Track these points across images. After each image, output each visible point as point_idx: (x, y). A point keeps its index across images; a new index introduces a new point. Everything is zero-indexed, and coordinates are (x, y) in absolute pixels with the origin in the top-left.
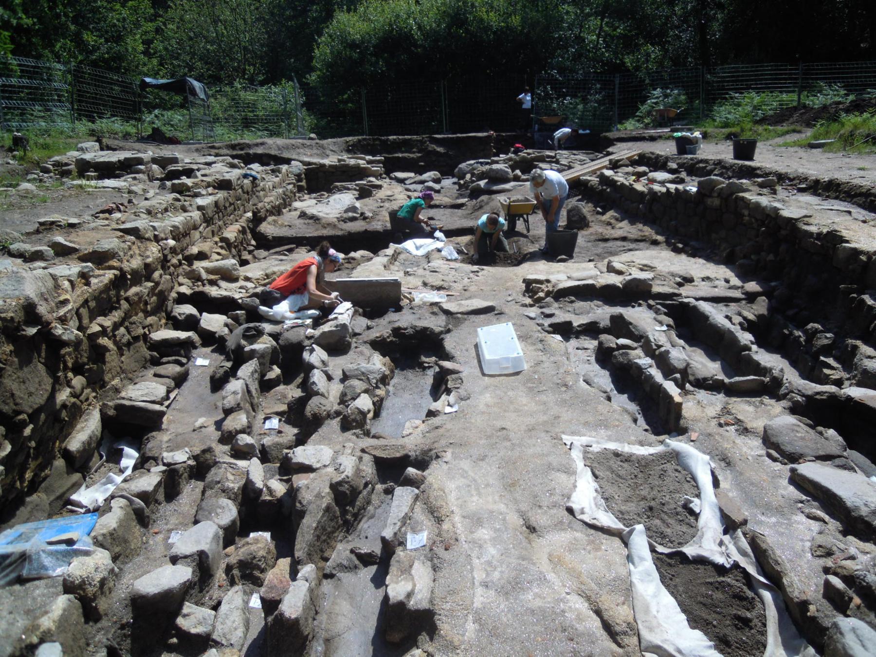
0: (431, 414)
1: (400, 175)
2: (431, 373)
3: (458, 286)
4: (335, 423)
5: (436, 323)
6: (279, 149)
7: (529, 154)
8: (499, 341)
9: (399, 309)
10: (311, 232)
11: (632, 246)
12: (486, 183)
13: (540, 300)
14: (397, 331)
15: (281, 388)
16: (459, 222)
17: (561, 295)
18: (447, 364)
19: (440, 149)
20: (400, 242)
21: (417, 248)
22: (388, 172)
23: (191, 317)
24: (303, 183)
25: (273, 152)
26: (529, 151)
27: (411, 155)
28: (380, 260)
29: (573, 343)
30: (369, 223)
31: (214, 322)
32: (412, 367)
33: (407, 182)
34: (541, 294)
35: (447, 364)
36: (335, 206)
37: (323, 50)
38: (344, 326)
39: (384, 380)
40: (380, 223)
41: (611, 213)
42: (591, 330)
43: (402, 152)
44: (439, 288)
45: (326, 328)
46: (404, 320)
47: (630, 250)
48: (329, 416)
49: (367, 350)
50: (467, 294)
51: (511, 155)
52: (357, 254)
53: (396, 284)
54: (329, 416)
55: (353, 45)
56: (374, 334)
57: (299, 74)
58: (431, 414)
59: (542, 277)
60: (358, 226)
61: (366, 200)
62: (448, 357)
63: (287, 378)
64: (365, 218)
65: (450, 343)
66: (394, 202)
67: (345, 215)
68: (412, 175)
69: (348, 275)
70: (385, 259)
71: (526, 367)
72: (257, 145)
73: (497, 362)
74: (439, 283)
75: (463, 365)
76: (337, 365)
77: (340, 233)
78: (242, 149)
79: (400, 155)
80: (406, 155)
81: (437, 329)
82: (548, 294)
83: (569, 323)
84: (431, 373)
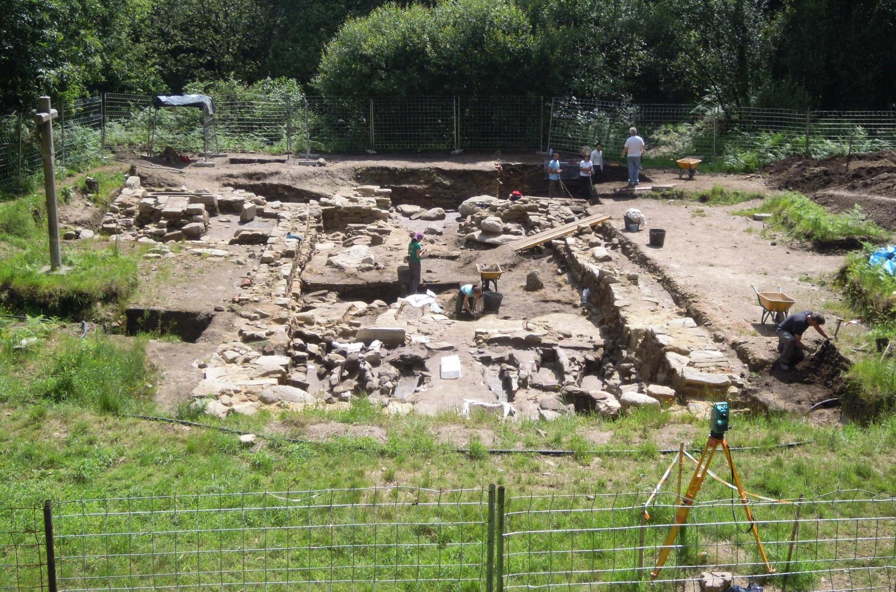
0: (416, 391)
1: (407, 208)
2: (418, 378)
3: (437, 333)
4: (378, 392)
5: (422, 354)
6: (293, 180)
7: (525, 202)
8: (450, 364)
9: (404, 345)
10: (339, 280)
11: (562, 306)
12: (481, 235)
13: (479, 344)
14: (402, 357)
15: (348, 380)
16: (450, 276)
17: (490, 342)
18: (425, 373)
19: (447, 183)
20: (404, 297)
21: (417, 301)
22: (396, 203)
23: (301, 345)
24: (321, 224)
25: (287, 183)
26: (526, 198)
27: (418, 187)
28: (392, 311)
29: (491, 367)
30: (382, 273)
31: (313, 348)
32: (409, 375)
33: (412, 217)
34: (481, 341)
35: (425, 373)
36: (354, 256)
37: (332, 53)
38: (378, 353)
39: (396, 379)
40: (389, 274)
41: (565, 277)
42: (500, 361)
43: (410, 183)
44: (427, 334)
45: (370, 354)
46: (406, 351)
47: (557, 311)
48: (375, 389)
49: (388, 365)
50: (442, 338)
51: (509, 202)
52: (377, 303)
53: (403, 332)
54: (375, 389)
55: (365, 59)
56: (391, 358)
57: (304, 74)
58: (416, 391)
59: (484, 331)
60: (372, 277)
61: (378, 247)
62: (426, 370)
63: (351, 376)
64: (378, 269)
65: (427, 364)
66: (400, 252)
67: (363, 266)
68: (417, 208)
69: (373, 322)
70: (395, 311)
71: (461, 376)
72: (272, 174)
73: (447, 373)
74: (426, 331)
75: (433, 374)
76: (376, 371)
77: (360, 282)
78: (258, 179)
79: (407, 186)
80: (413, 186)
81: (423, 357)
82: (484, 340)
83: (490, 357)
84: (418, 378)
